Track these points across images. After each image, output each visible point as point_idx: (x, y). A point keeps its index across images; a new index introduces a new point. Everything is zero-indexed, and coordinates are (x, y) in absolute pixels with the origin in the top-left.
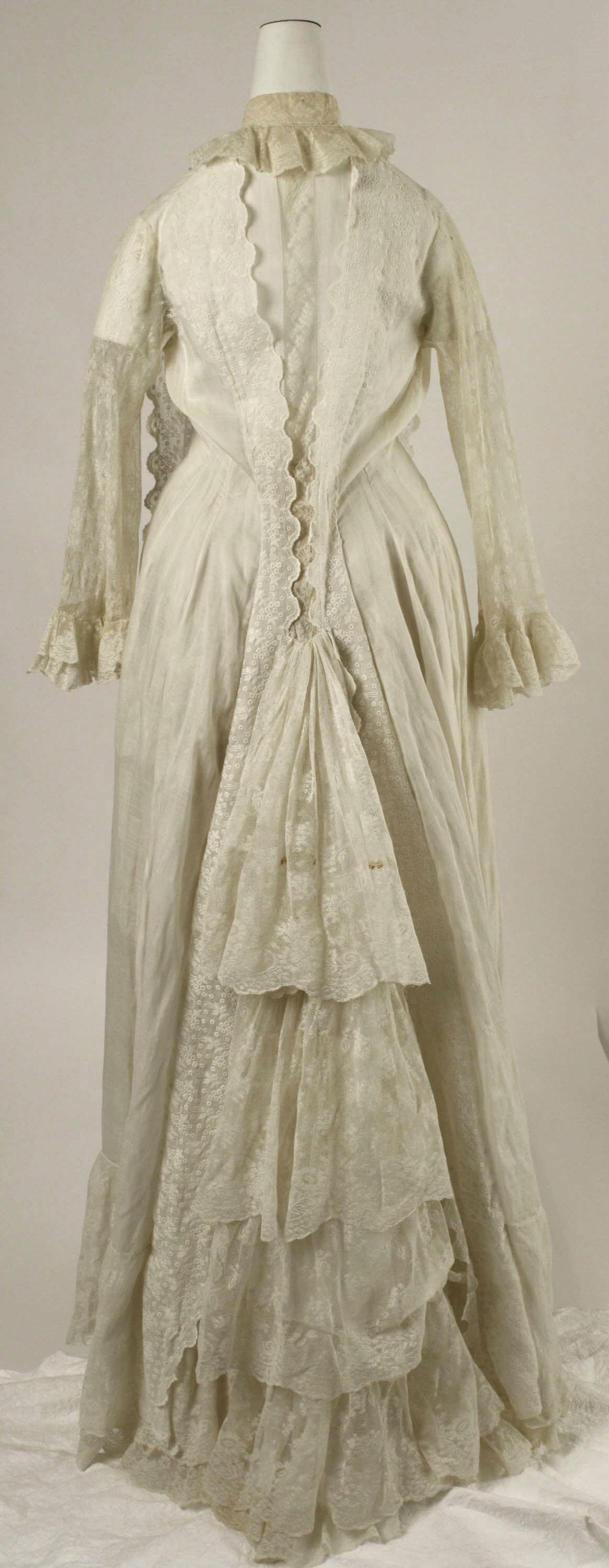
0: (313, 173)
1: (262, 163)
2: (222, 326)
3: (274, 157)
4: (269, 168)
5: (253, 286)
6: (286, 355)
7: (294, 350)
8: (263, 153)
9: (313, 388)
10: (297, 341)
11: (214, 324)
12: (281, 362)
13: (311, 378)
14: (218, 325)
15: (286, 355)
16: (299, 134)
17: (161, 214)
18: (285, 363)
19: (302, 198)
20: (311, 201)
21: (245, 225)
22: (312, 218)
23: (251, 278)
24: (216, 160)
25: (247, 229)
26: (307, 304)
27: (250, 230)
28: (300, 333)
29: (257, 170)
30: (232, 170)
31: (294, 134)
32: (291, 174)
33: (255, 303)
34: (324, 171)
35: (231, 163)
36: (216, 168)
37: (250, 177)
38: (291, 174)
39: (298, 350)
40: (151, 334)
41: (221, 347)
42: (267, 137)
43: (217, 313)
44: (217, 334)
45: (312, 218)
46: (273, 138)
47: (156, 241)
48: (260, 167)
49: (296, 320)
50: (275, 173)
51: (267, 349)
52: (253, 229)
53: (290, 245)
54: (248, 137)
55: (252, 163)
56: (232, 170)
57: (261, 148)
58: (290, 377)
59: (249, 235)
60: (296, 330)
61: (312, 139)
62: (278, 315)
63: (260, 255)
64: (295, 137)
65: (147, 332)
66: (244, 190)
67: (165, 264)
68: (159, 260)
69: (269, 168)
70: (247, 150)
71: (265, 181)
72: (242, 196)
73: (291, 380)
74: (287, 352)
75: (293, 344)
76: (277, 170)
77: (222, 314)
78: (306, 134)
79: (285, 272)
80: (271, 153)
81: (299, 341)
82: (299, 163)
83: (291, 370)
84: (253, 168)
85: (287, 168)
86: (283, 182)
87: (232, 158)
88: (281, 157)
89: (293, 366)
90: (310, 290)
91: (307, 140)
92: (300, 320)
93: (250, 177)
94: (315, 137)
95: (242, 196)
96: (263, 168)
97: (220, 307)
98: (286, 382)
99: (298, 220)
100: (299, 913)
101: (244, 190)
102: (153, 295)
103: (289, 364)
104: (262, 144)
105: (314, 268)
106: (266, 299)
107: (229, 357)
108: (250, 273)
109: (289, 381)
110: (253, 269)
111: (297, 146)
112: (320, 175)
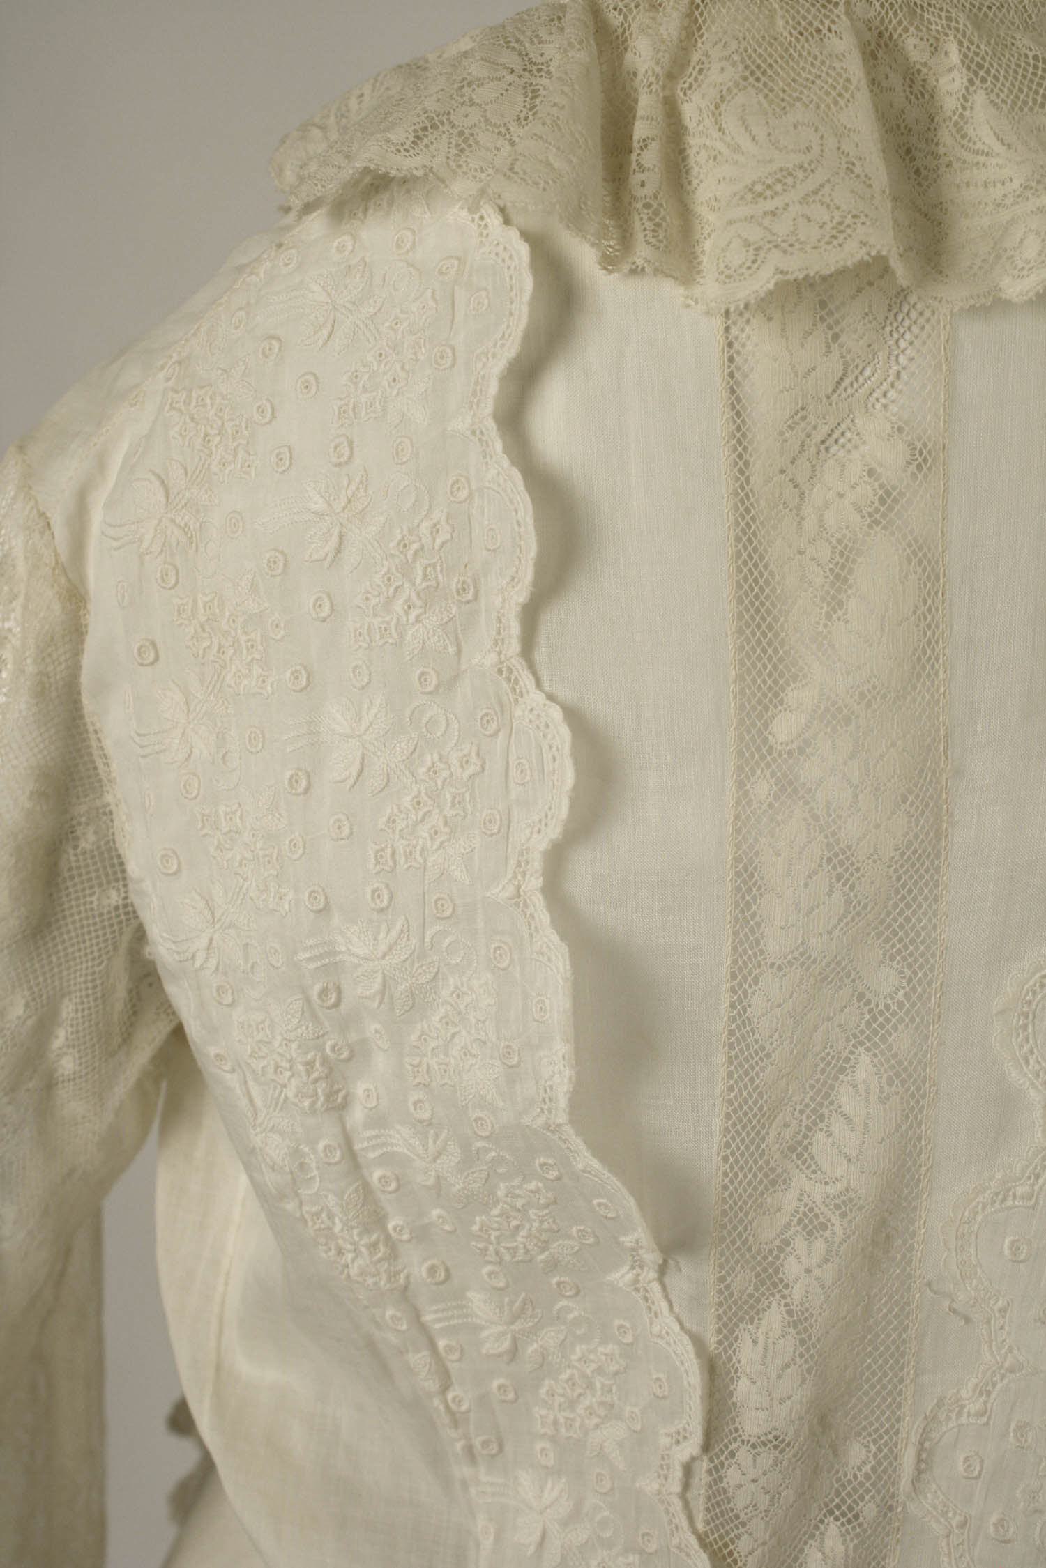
0: (954, 294)
1: (640, 224)
2: (378, 1121)
3: (711, 185)
4: (681, 254)
5: (552, 968)
6: (728, 1332)
7: (775, 1317)
8: (648, 159)
9: (869, 1510)
10: (792, 1267)
11: (338, 1105)
12: (693, 1377)
13: (857, 1454)
14: (357, 1115)
15: (728, 1332)
16: (878, 48)
17: (101, 464)
18: (716, 1375)
19: (874, 444)
20: (923, 459)
21: (520, 595)
22: (928, 568)
23: (538, 904)
24: (372, 190)
25: (531, 615)
26: (864, 1068)
27: (549, 623)
28: (812, 1224)
29: (608, 263)
30: (461, 253)
31: (843, 46)
32: (811, 299)
33: (556, 1068)
34: (1016, 288)
35: (458, 215)
36: (378, 235)
37: (561, 304)
38: (811, 299)
39: (797, 1320)
40: (60, 1038)
41: (377, 1220)
42: (677, 68)
43: (358, 1053)
44: (351, 1155)
45: (928, 568)
46: (717, 70)
47: (75, 598)
48: (626, 240)
49: (799, 1150)
50: (710, 288)
51: (622, 1276)
52: (565, 619)
53: (784, 729)
54: (566, 55)
55: (576, 220)
56: (461, 253)
57: (640, 130)
58: (744, 1456)
59: (541, 654)
60: (789, 1200)
61: (950, 83)
62: (691, 1117)
63: (601, 772)
64: (855, 68)
65: (44, 1025)
66: (525, 377)
67: (114, 723)
68: (86, 700)
69: (681, 254)
70: (558, 143)
71: (655, 337)
72: (514, 418)
73: (746, 1476)
74: (737, 1313)
75: (770, 1280)
76: (728, 276)
77: (381, 1062)
78: (913, 47)
79: (747, 881)
80: (698, 158)
81: (808, 1268)
82: (878, 236)
83: (752, 1422)
84: (584, 256)
85: (796, 266)
86: (764, 349)
87: (461, 186)
88: (754, 193)
89: (768, 1394)
90: (885, 981)
91: (917, 85)
92: (820, 1144)
93: (561, 304)
94: (974, 67)
95: (514, 418)
96: (642, 252)
97: (372, 1027)
98: (716, 1472)
99: (840, 576)
100: (775, 259)
101: (525, 377)
102: (70, 856)
103: (743, 1389)
104: (647, 104)
105: (920, 864)
106: (623, 1016)
107: (417, 1266)
108: (535, 883)
109: (732, 1476)
110: (557, 861)
111: (859, 121)
112: (993, 306)
